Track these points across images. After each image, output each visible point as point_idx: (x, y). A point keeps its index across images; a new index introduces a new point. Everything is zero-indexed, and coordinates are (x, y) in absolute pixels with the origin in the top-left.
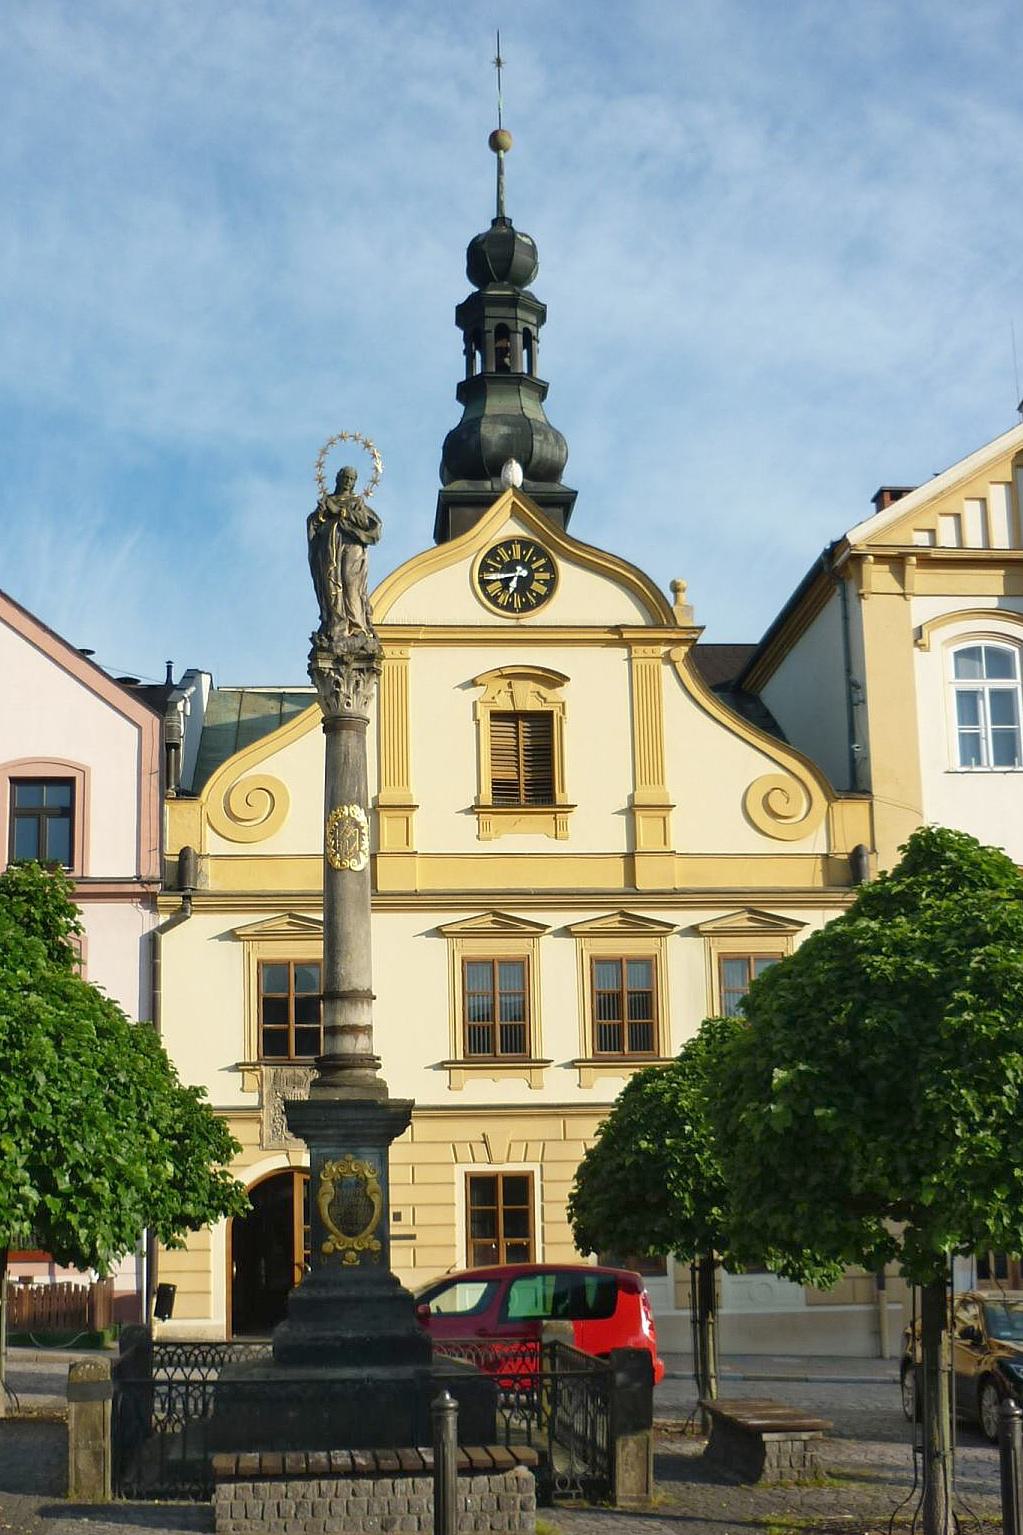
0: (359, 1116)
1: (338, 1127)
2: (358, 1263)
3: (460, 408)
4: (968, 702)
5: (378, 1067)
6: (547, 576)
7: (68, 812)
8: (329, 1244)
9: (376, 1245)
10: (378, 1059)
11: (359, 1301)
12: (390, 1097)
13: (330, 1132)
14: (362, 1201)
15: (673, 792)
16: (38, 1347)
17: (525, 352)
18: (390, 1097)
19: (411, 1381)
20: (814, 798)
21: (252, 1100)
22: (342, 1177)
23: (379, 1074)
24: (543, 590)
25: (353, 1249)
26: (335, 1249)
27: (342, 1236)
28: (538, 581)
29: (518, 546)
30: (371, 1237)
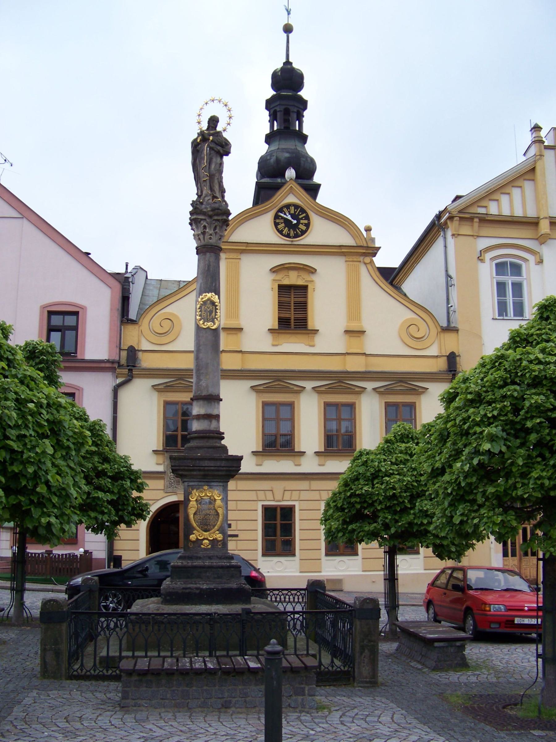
0: (212, 465)
1: (200, 470)
2: (210, 547)
3: (267, 146)
4: (501, 287)
5: (223, 438)
6: (306, 222)
7: (75, 328)
8: (194, 536)
9: (219, 537)
10: (223, 433)
11: (211, 567)
12: (230, 454)
13: (195, 473)
14: (213, 512)
15: (366, 325)
16: (56, 584)
17: (297, 122)
18: (230, 454)
19: (240, 614)
20: (430, 327)
21: (161, 469)
22: (202, 498)
23: (223, 442)
24: (304, 228)
25: (207, 539)
26: (197, 539)
27: (201, 531)
28: (302, 224)
29: (293, 207)
30: (217, 532)
